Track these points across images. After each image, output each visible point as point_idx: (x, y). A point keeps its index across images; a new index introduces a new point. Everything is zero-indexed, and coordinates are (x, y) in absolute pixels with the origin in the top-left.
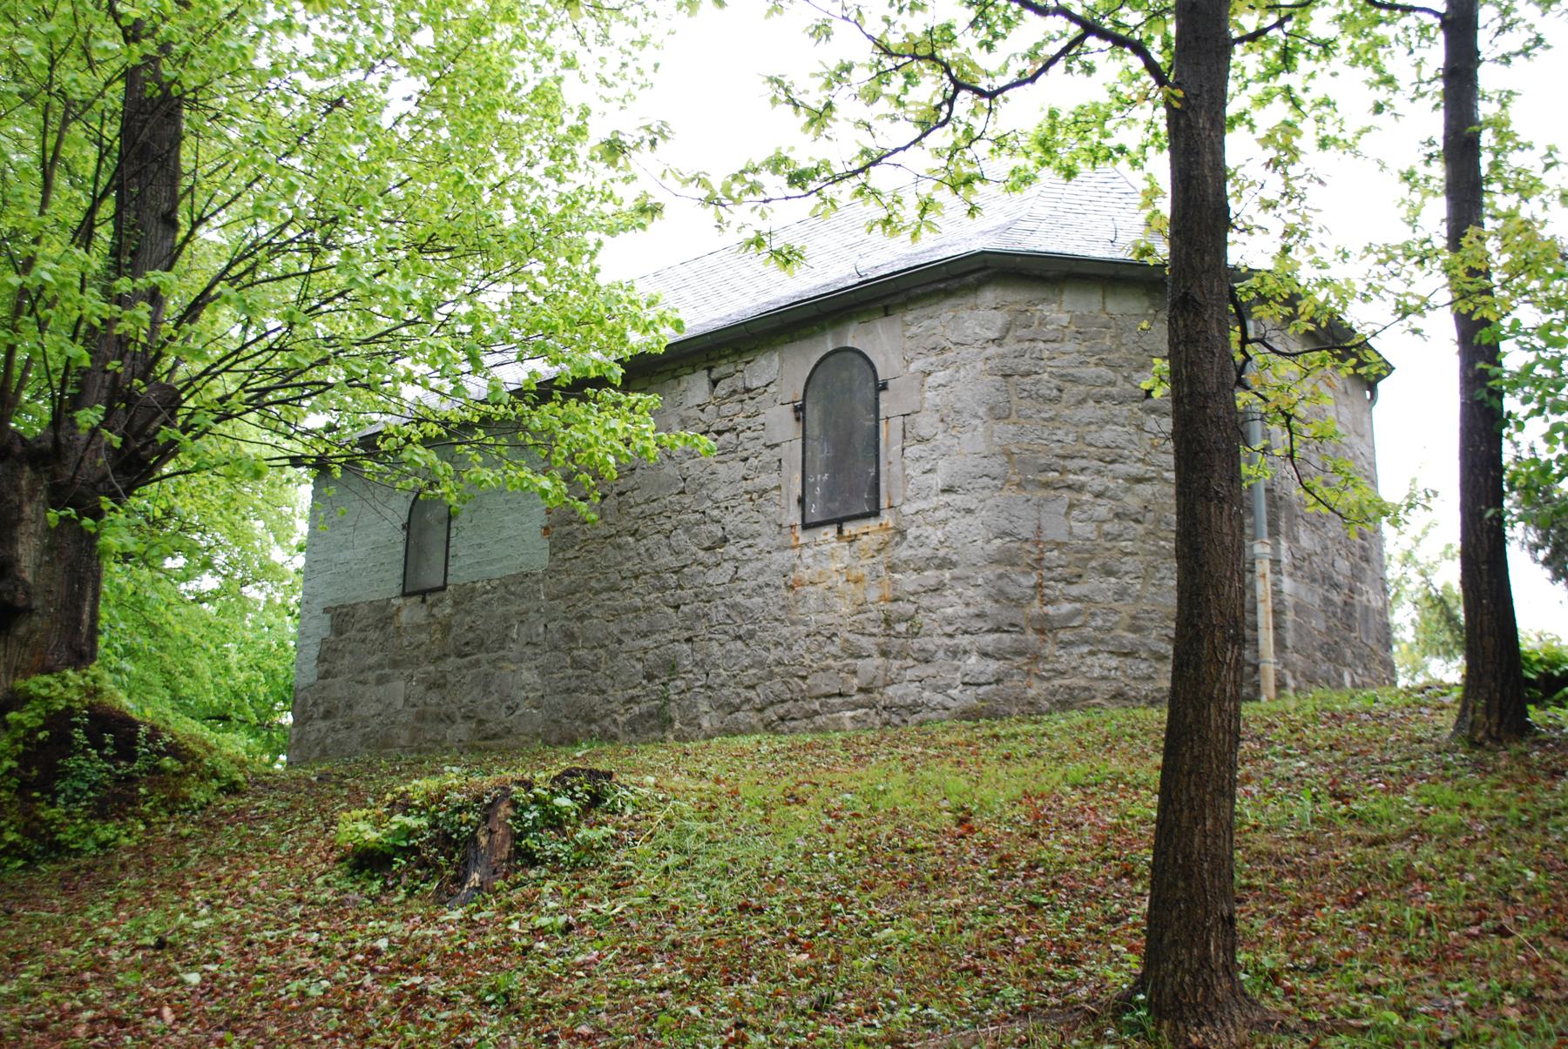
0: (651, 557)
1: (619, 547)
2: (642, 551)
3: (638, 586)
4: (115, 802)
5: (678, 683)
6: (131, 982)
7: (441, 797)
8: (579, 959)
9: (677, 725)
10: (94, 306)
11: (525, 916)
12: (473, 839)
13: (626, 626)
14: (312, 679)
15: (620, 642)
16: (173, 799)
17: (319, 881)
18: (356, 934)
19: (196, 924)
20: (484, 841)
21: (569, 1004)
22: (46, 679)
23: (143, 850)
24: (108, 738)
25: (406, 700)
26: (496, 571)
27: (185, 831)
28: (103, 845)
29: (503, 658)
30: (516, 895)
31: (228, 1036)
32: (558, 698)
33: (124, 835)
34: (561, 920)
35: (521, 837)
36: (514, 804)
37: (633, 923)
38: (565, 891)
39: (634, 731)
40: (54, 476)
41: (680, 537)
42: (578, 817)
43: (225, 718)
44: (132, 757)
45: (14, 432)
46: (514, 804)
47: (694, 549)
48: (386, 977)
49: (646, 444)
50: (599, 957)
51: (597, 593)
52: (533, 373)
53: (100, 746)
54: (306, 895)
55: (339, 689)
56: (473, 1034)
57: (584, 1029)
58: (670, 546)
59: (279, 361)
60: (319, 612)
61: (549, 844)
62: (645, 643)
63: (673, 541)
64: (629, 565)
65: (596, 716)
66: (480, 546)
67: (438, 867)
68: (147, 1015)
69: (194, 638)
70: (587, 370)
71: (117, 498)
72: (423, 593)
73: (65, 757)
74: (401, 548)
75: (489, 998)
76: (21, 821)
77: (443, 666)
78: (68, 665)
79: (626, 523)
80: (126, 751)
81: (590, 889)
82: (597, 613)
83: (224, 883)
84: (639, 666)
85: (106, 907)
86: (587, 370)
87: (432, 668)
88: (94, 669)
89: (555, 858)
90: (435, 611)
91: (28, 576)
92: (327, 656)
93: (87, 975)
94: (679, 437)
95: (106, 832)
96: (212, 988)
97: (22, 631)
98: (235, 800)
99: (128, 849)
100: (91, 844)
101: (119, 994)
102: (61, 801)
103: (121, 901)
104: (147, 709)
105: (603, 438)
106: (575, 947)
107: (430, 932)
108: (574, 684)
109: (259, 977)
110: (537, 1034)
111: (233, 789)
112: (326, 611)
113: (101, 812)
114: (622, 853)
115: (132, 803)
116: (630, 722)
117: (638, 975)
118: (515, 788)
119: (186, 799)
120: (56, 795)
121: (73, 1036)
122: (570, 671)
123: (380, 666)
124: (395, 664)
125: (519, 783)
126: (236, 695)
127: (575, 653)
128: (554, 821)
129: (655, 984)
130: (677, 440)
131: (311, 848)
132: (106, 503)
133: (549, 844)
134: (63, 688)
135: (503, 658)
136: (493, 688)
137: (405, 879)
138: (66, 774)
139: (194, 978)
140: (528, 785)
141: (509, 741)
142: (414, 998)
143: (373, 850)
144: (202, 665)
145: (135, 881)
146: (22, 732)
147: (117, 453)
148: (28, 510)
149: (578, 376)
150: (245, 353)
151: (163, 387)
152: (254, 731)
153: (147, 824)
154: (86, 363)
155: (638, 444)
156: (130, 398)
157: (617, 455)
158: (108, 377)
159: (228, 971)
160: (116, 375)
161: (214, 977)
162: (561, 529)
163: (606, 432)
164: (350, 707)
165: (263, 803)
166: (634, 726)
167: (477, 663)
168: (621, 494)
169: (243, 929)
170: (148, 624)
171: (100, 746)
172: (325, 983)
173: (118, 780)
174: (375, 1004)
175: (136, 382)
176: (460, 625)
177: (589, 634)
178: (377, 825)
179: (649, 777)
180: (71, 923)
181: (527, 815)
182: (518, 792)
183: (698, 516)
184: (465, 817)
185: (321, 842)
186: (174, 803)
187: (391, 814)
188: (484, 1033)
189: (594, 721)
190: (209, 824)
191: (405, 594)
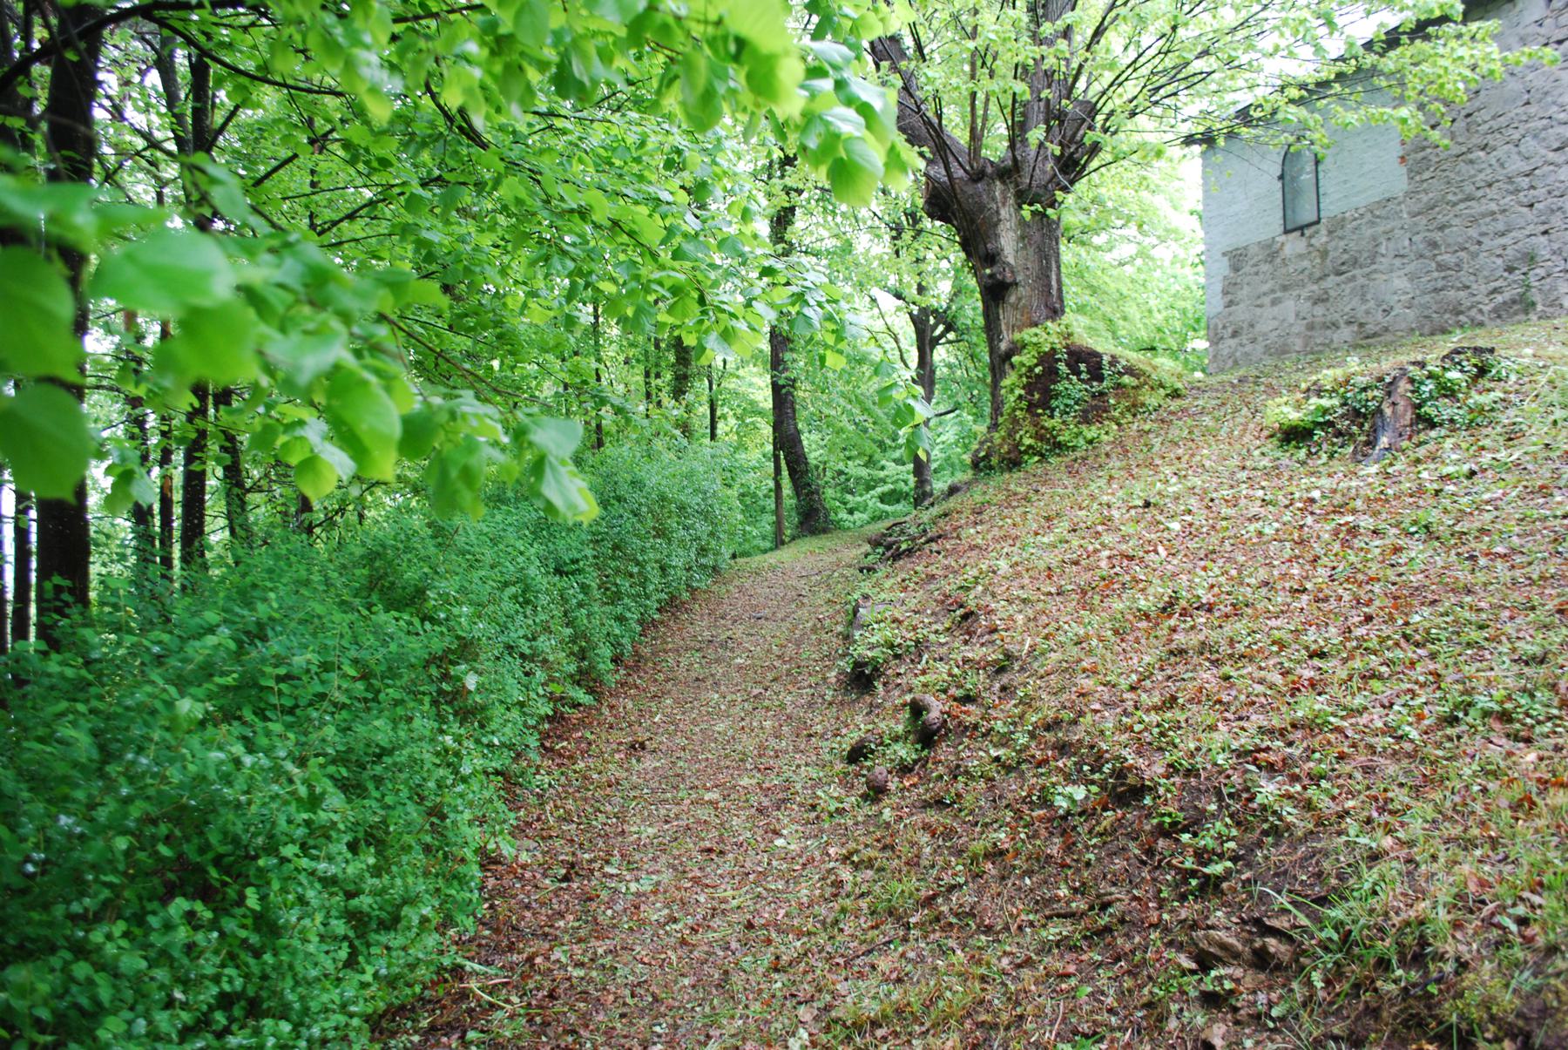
0: (1502, 165)
1: (1471, 162)
2: (1493, 161)
3: (1491, 193)
4: (1094, 411)
5: (1538, 271)
6: (1131, 531)
7: (1347, 382)
8: (1486, 496)
9: (1539, 307)
10: (1027, 52)
11: (1432, 466)
12: (1379, 411)
13: (1484, 229)
14: (1220, 308)
15: (1479, 243)
16: (1134, 406)
17: (1256, 453)
18: (1292, 489)
19: (1171, 489)
20: (1388, 411)
21: (1483, 531)
22: (1034, 330)
23: (1119, 443)
24: (1083, 367)
25: (1297, 315)
26: (1362, 201)
27: (1147, 427)
28: (1090, 442)
29: (1375, 271)
30: (1422, 452)
31: (1209, 564)
32: (1427, 298)
33: (1102, 433)
34: (1466, 468)
35: (1419, 406)
36: (1412, 381)
37: (1529, 467)
38: (1464, 445)
39: (1499, 317)
40: (1017, 185)
41: (1530, 144)
42: (1468, 387)
43: (1153, 349)
44: (1101, 379)
45: (986, 159)
46: (1412, 381)
47: (1543, 152)
48: (1325, 517)
49: (1492, 66)
50: (1504, 494)
51: (1455, 204)
52: (1381, 25)
53: (1078, 373)
54: (1248, 464)
55: (1241, 313)
56: (1404, 556)
57: (1500, 549)
58: (1519, 153)
59: (1169, 62)
60: (1219, 256)
61: (1444, 409)
62: (1503, 241)
63: (1522, 148)
64: (1482, 176)
65: (1462, 308)
66: (1345, 182)
67: (1352, 435)
68: (1147, 552)
69: (1125, 292)
70: (1432, 11)
71: (1065, 189)
72: (1301, 229)
73: (1055, 383)
74: (1279, 195)
75: (1413, 529)
76: (1032, 430)
77: (1324, 284)
78: (1047, 318)
79: (1476, 140)
80: (1096, 374)
81: (1486, 442)
82: (1454, 222)
83: (1184, 460)
84: (1499, 261)
85: (1102, 482)
86: (1432, 11)
87: (1315, 287)
88: (1065, 319)
89: (1452, 421)
90: (1313, 241)
91: (1011, 260)
92: (1229, 290)
93: (1100, 528)
94: (1523, 53)
95: (1091, 432)
96: (1190, 531)
97: (1013, 299)
98: (1178, 402)
99: (1108, 443)
100: (1081, 442)
101: (1125, 539)
102: (1057, 413)
103: (1111, 477)
104: (1103, 345)
105: (1451, 68)
106: (1481, 488)
107: (1353, 484)
108: (1440, 284)
109: (1224, 523)
110: (1458, 554)
111: (1176, 394)
112: (1224, 254)
113: (1086, 419)
114: (1512, 412)
115: (1106, 411)
116: (1495, 310)
117: (1541, 506)
118: (1411, 368)
119: (1143, 405)
120: (1053, 410)
121: (1098, 567)
122: (1436, 274)
123: (1273, 291)
124: (1285, 288)
125: (1414, 363)
126: (1159, 330)
127: (1439, 258)
128: (1448, 392)
129: (1558, 513)
130: (1520, 56)
131: (1245, 430)
132: (1059, 195)
133: (1444, 409)
134: (1047, 336)
135: (1375, 271)
136: (1369, 297)
137: (1325, 446)
138: (1057, 395)
139: (1175, 526)
140: (1422, 365)
141: (1388, 337)
142: (1349, 532)
143: (1296, 427)
144: (1132, 310)
145: (1118, 464)
146: (1024, 370)
147: (1057, 159)
148: (1004, 213)
149: (1423, 18)
150: (1142, 60)
151: (1082, 103)
152: (1173, 354)
153: (1119, 424)
154: (1028, 97)
155: (1484, 67)
156: (1061, 116)
157: (1465, 80)
158: (1042, 104)
159: (1200, 518)
160: (1048, 101)
161: (1191, 525)
162: (1417, 157)
163: (1454, 61)
164: (1252, 326)
165: (1200, 402)
166: (1498, 313)
167: (1354, 278)
168: (1469, 115)
169: (1205, 491)
170: (1091, 286)
171: (1078, 373)
172: (1276, 525)
173: (1094, 396)
174: (1319, 537)
175: (1064, 102)
176: (1336, 249)
177: (1450, 241)
178: (1298, 407)
179: (1520, 349)
180: (1080, 495)
181: (1423, 388)
182: (1415, 372)
183: (1545, 122)
184: (1370, 394)
185: (1252, 426)
186: (1135, 408)
187: (1308, 398)
188: (1413, 555)
189: (1461, 313)
190: (1163, 421)
191: (1286, 232)
